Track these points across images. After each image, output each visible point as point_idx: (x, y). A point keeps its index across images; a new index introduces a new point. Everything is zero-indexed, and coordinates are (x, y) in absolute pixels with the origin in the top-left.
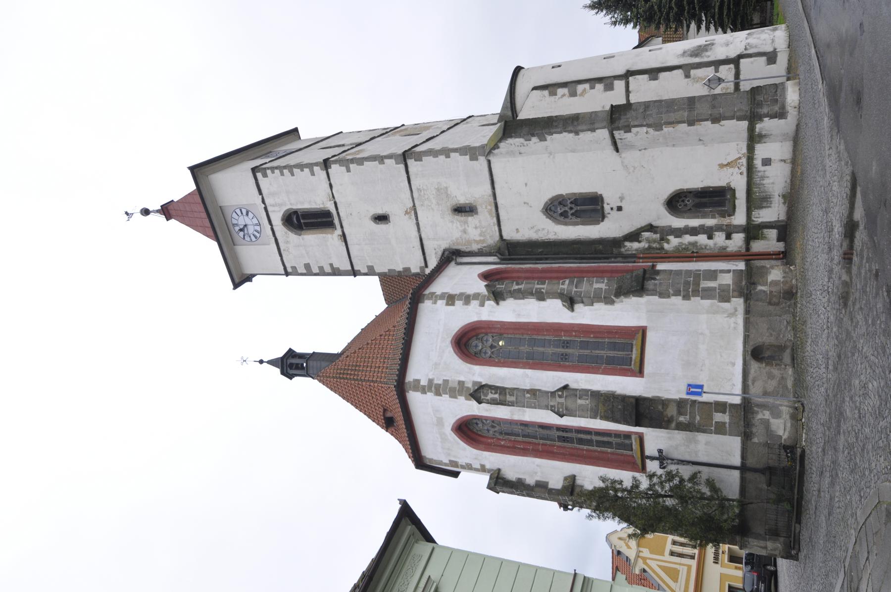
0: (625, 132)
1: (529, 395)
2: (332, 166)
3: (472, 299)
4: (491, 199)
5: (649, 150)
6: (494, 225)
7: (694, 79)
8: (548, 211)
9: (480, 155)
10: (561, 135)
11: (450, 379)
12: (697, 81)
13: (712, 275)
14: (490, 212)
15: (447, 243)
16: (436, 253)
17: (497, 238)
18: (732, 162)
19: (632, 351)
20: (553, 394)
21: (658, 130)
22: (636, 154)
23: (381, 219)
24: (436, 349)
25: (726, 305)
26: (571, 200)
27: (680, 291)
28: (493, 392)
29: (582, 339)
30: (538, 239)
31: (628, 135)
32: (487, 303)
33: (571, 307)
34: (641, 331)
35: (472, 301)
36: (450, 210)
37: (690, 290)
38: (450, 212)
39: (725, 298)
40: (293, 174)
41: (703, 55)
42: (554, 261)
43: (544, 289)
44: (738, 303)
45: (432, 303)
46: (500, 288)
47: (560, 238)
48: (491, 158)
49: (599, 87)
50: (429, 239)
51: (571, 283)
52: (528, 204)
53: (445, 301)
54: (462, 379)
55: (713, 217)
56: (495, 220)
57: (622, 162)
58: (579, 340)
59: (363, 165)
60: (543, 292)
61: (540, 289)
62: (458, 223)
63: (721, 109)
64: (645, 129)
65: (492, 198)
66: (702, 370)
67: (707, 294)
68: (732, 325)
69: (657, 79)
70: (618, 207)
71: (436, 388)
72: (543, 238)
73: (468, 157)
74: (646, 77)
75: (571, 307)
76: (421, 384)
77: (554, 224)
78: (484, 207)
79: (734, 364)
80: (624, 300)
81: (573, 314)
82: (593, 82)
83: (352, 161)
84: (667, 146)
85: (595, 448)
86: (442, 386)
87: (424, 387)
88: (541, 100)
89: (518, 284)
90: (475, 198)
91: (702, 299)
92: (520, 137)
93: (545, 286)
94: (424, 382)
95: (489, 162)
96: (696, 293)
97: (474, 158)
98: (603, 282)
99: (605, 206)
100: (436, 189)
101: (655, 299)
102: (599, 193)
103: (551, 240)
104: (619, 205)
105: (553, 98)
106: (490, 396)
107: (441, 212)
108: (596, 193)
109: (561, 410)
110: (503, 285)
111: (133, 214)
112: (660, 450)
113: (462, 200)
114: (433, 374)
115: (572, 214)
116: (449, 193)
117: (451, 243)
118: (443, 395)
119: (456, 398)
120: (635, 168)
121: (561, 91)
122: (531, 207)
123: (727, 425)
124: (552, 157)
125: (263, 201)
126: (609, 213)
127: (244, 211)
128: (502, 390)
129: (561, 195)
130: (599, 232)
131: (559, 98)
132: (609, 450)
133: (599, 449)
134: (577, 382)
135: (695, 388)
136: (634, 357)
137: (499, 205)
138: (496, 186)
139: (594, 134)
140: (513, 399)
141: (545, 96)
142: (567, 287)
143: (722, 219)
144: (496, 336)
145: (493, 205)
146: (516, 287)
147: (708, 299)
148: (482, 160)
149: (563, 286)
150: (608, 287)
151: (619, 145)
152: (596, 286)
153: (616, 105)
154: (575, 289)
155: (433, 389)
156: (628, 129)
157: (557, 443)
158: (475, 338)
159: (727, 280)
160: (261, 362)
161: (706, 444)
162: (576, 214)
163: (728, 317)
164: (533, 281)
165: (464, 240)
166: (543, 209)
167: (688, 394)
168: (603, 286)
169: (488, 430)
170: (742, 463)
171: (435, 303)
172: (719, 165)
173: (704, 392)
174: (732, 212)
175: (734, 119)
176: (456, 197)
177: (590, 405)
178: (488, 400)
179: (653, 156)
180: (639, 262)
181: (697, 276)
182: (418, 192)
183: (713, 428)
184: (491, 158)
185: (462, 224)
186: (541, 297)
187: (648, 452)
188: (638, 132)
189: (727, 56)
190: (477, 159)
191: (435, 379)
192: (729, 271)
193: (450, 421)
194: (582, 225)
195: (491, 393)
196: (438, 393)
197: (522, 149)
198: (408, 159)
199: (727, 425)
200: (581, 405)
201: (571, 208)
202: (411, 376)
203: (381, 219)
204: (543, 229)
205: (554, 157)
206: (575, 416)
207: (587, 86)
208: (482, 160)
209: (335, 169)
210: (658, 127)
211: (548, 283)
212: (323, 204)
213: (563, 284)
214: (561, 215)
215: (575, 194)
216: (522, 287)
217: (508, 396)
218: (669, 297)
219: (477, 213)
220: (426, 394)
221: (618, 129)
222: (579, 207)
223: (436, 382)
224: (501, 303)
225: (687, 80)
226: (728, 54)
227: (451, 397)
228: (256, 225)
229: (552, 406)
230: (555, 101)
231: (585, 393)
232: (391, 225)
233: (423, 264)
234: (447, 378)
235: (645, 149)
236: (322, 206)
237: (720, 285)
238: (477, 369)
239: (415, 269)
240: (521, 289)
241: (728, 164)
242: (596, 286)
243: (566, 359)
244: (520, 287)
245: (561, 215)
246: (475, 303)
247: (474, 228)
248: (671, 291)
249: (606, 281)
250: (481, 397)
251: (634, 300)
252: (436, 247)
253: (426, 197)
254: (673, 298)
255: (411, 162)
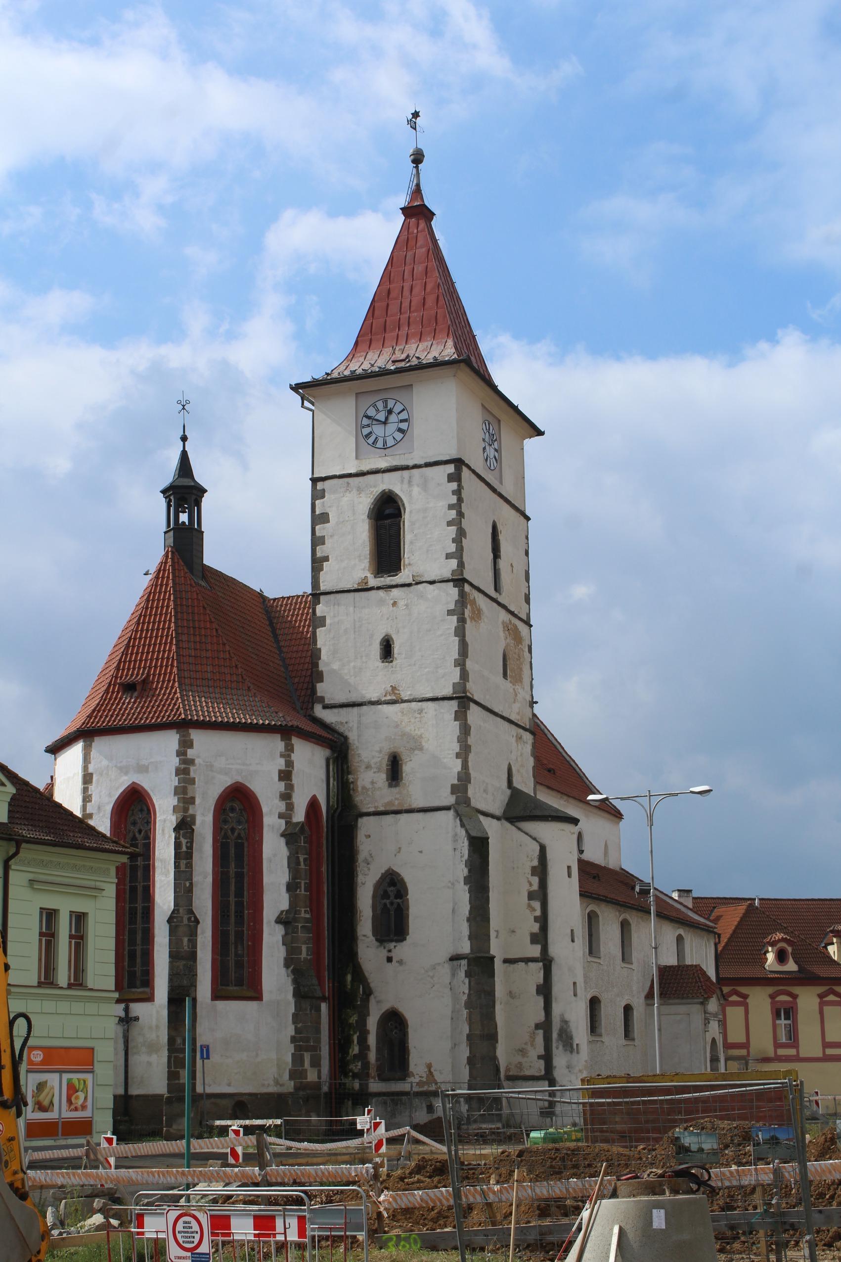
0: (466, 971)
1: (188, 885)
2: (457, 589)
3: (286, 803)
4: (406, 807)
5: (450, 993)
6: (375, 807)
7: (534, 1033)
8: (390, 876)
9: (457, 798)
10: (468, 903)
11: (196, 786)
12: (531, 1037)
13: (316, 1063)
14: (390, 803)
15: (354, 740)
16: (342, 723)
17: (365, 810)
18: (433, 1076)
19: (235, 986)
20: (191, 912)
21: (465, 1004)
22: (447, 979)
23: (387, 650)
24: (229, 764)
25: (286, 1076)
26: (401, 904)
27: (300, 1034)
28: (189, 845)
29: (245, 932)
30: (357, 861)
31: (462, 974)
32: (283, 822)
33: (279, 921)
34: (257, 995)
35: (284, 803)
36: (395, 750)
37: (301, 1043)
38: (393, 750)
39: (293, 1075)
40: (449, 524)
41: (560, 1042)
42: (330, 883)
43: (300, 891)
44: (289, 1086)
45: (281, 752)
46: (301, 840)
47: (358, 889)
48: (451, 813)
49: (536, 928)
50: (360, 717)
51: (307, 920)
52: (399, 852)
53: (283, 768)
54: (198, 801)
55: (377, 1059)
56: (382, 809)
57: (439, 964)
58: (245, 929)
59: (456, 636)
60: (297, 891)
61: (300, 887)
62: (380, 759)
63: (480, 1065)
64: (467, 991)
65: (408, 808)
66: (222, 1056)
67: (297, 1059)
68: (266, 1083)
69: (537, 993)
70: (392, 957)
71: (185, 769)
72: (358, 869)
73: (456, 782)
74: (541, 981)
75: (279, 921)
76: (188, 750)
77: (375, 882)
78: (398, 796)
79: (229, 1085)
80: (290, 978)
81: (273, 923)
82: (543, 920)
83: (462, 620)
84: (452, 1012)
85: (127, 948)
86: (188, 777)
87: (185, 754)
88: (528, 856)
89: (305, 860)
90: (409, 786)
91: (292, 1054)
92: (469, 856)
93: (303, 892)
94: (190, 753)
95: (447, 808)
96: (298, 1049)
97: (454, 789)
98: (307, 955)
99: (394, 944)
100: (421, 735)
101: (292, 1009)
102: (408, 937)
103: (355, 879)
104: (394, 960)
105: (529, 871)
106: (184, 841)
107: (393, 737)
108: (408, 934)
109: (175, 920)
110: (304, 843)
111: (415, 129)
112: (138, 1019)
113: (407, 768)
114: (200, 764)
115: (385, 905)
116: (416, 752)
117: (355, 747)
118: (177, 778)
119: (175, 794)
120: (432, 977)
121: (535, 881)
122: (395, 855)
123: (177, 1082)
124: (450, 885)
125: (416, 467)
126: (385, 948)
127: (404, 426)
128: (189, 855)
129: (407, 894)
130: (364, 936)
131: (528, 878)
132: (126, 964)
133: (126, 952)
134: (203, 933)
135: (206, 1052)
136: (231, 988)
137: (399, 816)
138: (420, 815)
139: (467, 938)
140: (183, 868)
141: (532, 861)
142: (302, 917)
143: (375, 1069)
144: (245, 833)
145: (400, 808)
146: (302, 860)
147: (292, 1060)
148: (451, 800)
149: (303, 912)
150: (302, 960)
151: (455, 963)
152: (304, 948)
153: (494, 961)
154: (300, 925)
155: (183, 766)
156: (468, 974)
157: (127, 906)
158: (242, 808)
159: (312, 1076)
160: (184, 439)
161: (148, 1062)
162: (385, 908)
163: (274, 1078)
164: (308, 877)
165: (358, 764)
166: (392, 870)
167: (201, 1046)
168: (304, 955)
169: (134, 823)
170: (131, 1096)
171: (282, 756)
172: (431, 1063)
173: (203, 1061)
174: (382, 1078)
175: (470, 1077)
176: (411, 760)
177: (183, 950)
178: (179, 839)
179: (443, 997)
180: (329, 984)
181: (315, 1049)
182: (419, 710)
183: (173, 1069)
184: (451, 813)
185: (378, 764)
186: (291, 887)
187: (133, 1006)
188: (465, 984)
189: (555, 1067)
190: (452, 793)
191: (195, 768)
192: (319, 1077)
193: (145, 783)
194: (373, 916)
195: (187, 843)
196: (178, 772)
197: (458, 853)
198: (459, 702)
199: (177, 1082)
200: (182, 941)
201: (392, 904)
202: (196, 735)
203: (387, 650)
204: (369, 869)
205: (449, 887)
206: (170, 935)
207: (538, 913)
208: (451, 800)
209: (453, 592)
210: (469, 1005)
211: (306, 895)
212: (410, 564)
213: (305, 912)
214: (385, 892)
215: (408, 909)
216: (302, 866)
217: (185, 862)
218: (294, 1022)
219: (390, 786)
220: (177, 756)
221: (469, 965)
222: (393, 912)
223: (192, 768)
224: (283, 841)
225: (533, 1026)
226: (557, 1069)
227: (176, 788)
228: (385, 443)
229: (178, 910)
230: (525, 873)
231: (193, 943)
232: (379, 664)
233: (327, 702)
234: (196, 783)
235: (451, 989)
236: (407, 562)
237: (306, 1070)
238: (210, 818)
239: (321, 689)
240: (300, 866)
241: (431, 1073)
242: (304, 948)
243: (224, 915)
244: (302, 863)
245: (385, 892)
246: (282, 807)
247: (373, 780)
248: (299, 1025)
249: (309, 957)
250: (182, 830)
251: (290, 989)
252: (350, 725)
253: (413, 720)
254: (293, 1027)
255: (454, 705)
